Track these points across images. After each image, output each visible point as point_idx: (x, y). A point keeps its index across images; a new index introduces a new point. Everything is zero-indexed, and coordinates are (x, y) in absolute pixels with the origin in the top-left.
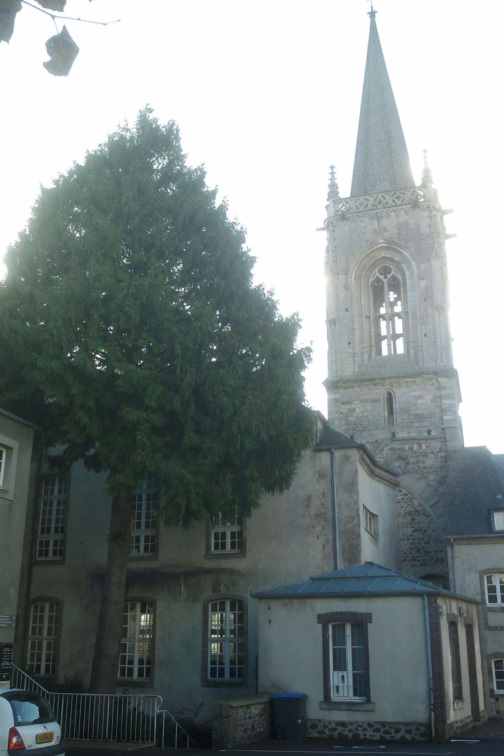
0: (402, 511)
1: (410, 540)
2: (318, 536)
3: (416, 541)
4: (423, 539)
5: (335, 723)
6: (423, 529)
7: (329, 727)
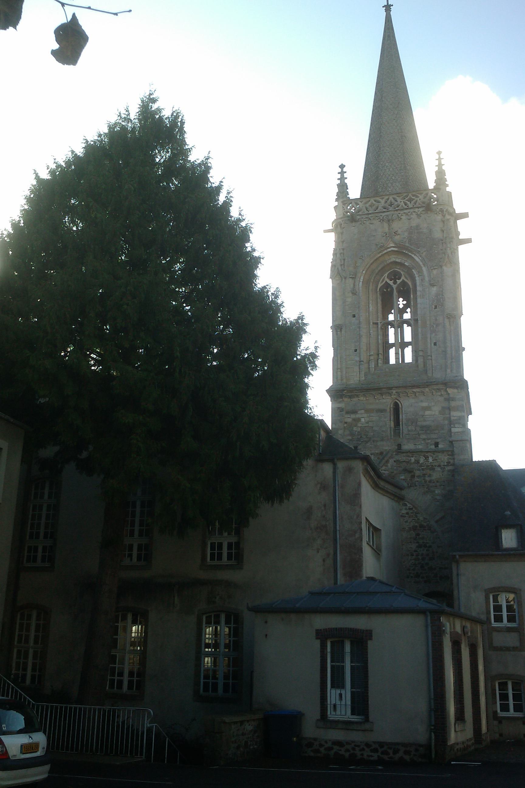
6: (428, 545)
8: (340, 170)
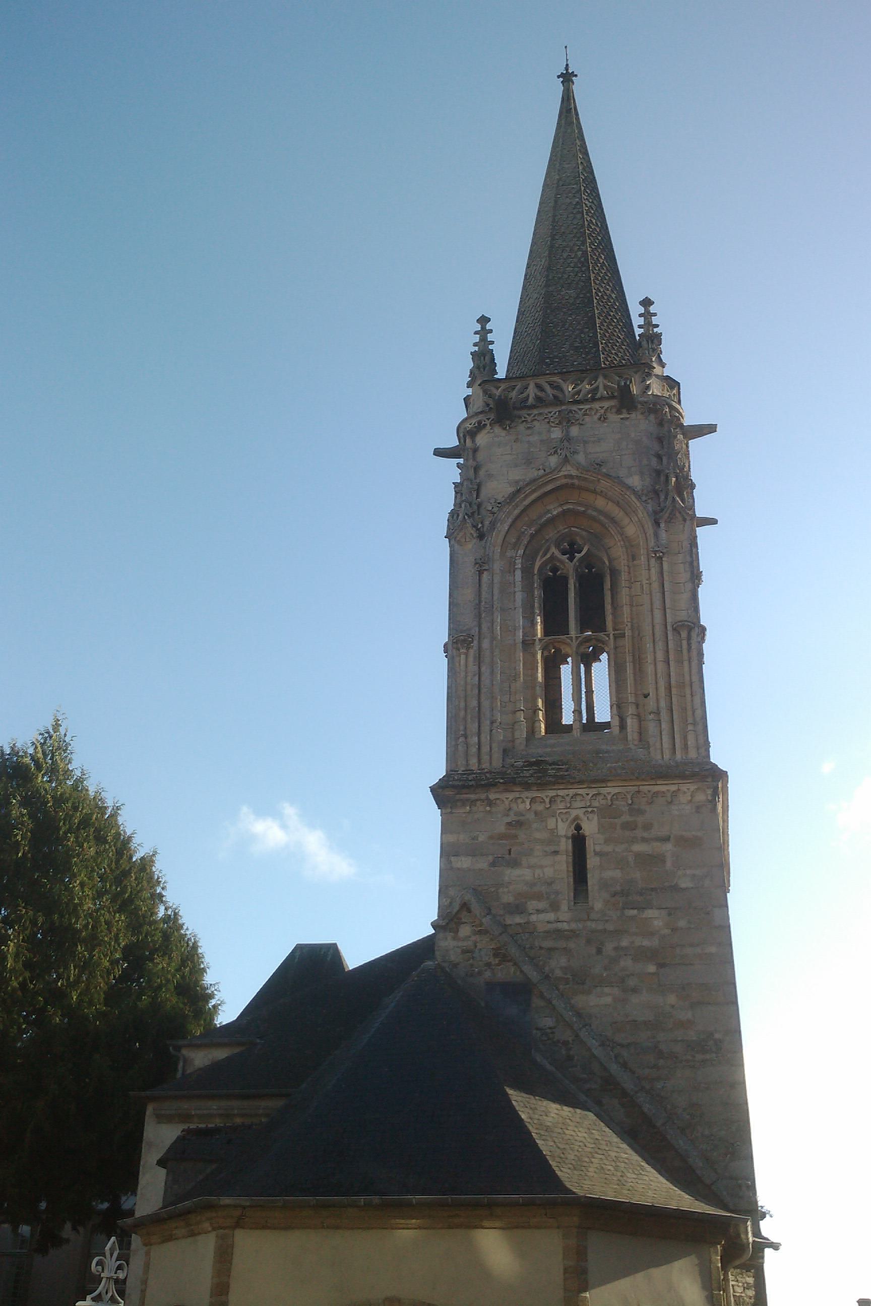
8: (478, 327)
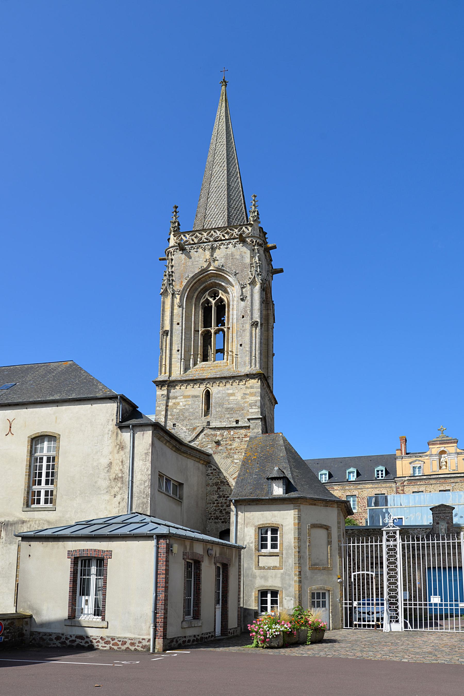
0: (210, 482)
1: (215, 503)
2: (115, 495)
3: (220, 505)
4: (226, 503)
5: (75, 636)
6: (226, 496)
7: (70, 640)
